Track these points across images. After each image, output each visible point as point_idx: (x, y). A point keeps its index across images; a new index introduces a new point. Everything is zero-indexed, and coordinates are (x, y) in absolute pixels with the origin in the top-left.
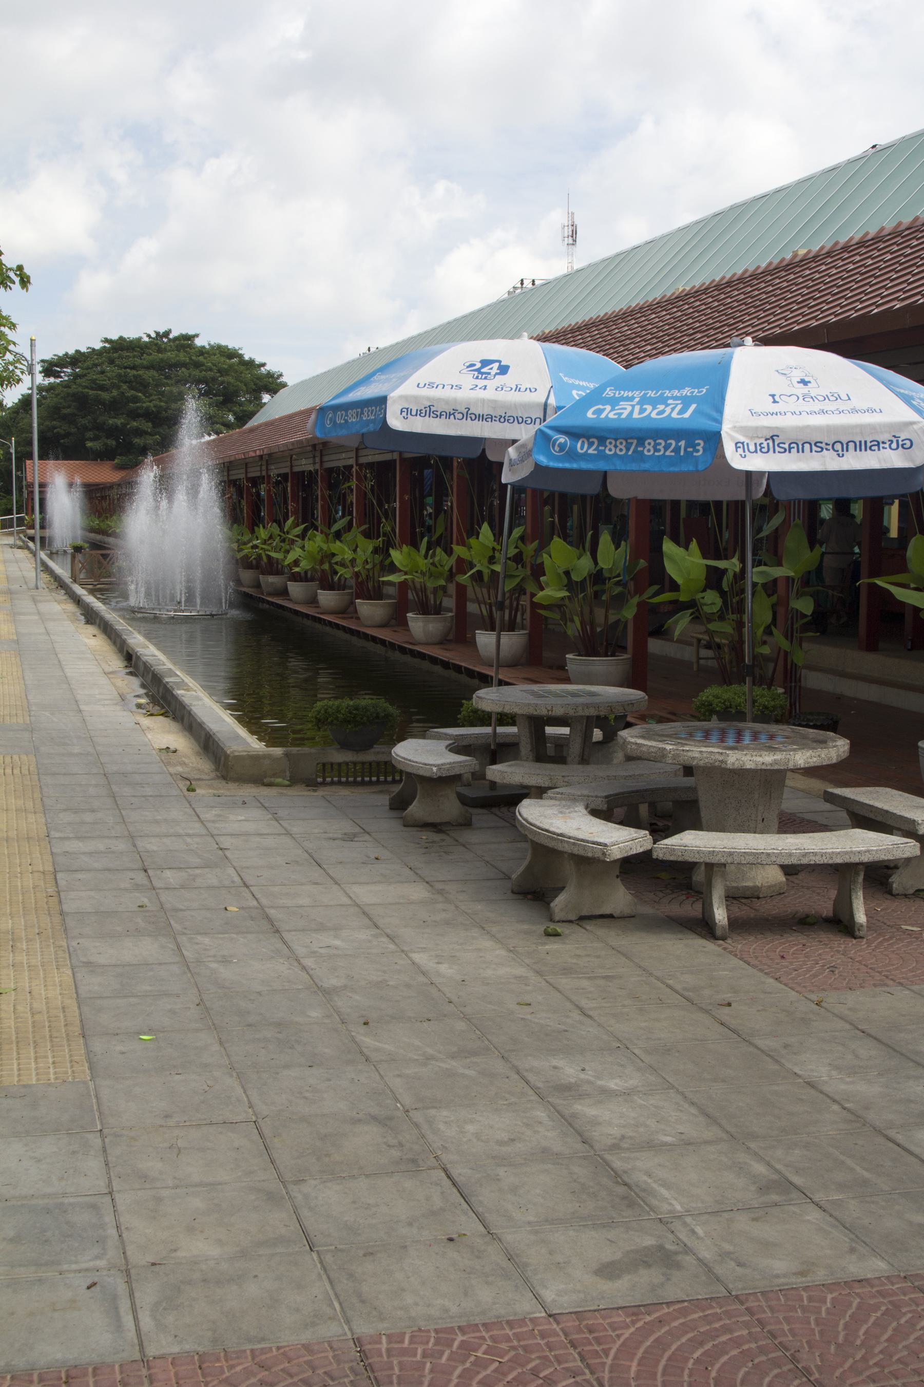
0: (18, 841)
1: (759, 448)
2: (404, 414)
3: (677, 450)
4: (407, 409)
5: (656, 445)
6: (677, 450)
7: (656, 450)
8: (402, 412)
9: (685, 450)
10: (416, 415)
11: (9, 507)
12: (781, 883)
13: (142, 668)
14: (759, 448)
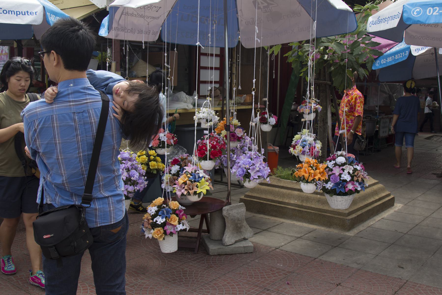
0: (277, 292)
1: (422, 49)
2: (417, 51)
3: (402, 56)
4: (418, 49)
5: (398, 55)
6: (402, 56)
7: (398, 57)
8: (416, 51)
9: (404, 55)
10: (422, 50)
11: (256, 105)
12: (402, 207)
13: (240, 127)
14: (422, 49)
